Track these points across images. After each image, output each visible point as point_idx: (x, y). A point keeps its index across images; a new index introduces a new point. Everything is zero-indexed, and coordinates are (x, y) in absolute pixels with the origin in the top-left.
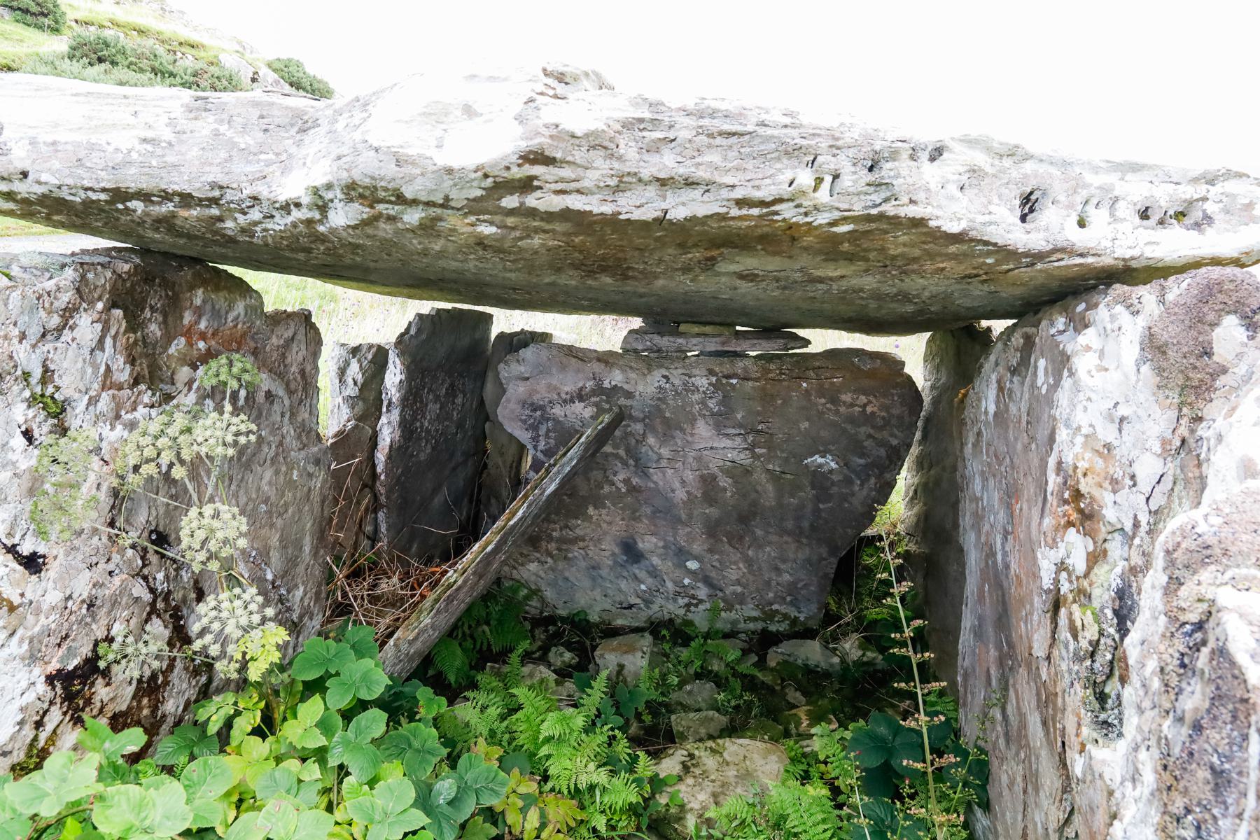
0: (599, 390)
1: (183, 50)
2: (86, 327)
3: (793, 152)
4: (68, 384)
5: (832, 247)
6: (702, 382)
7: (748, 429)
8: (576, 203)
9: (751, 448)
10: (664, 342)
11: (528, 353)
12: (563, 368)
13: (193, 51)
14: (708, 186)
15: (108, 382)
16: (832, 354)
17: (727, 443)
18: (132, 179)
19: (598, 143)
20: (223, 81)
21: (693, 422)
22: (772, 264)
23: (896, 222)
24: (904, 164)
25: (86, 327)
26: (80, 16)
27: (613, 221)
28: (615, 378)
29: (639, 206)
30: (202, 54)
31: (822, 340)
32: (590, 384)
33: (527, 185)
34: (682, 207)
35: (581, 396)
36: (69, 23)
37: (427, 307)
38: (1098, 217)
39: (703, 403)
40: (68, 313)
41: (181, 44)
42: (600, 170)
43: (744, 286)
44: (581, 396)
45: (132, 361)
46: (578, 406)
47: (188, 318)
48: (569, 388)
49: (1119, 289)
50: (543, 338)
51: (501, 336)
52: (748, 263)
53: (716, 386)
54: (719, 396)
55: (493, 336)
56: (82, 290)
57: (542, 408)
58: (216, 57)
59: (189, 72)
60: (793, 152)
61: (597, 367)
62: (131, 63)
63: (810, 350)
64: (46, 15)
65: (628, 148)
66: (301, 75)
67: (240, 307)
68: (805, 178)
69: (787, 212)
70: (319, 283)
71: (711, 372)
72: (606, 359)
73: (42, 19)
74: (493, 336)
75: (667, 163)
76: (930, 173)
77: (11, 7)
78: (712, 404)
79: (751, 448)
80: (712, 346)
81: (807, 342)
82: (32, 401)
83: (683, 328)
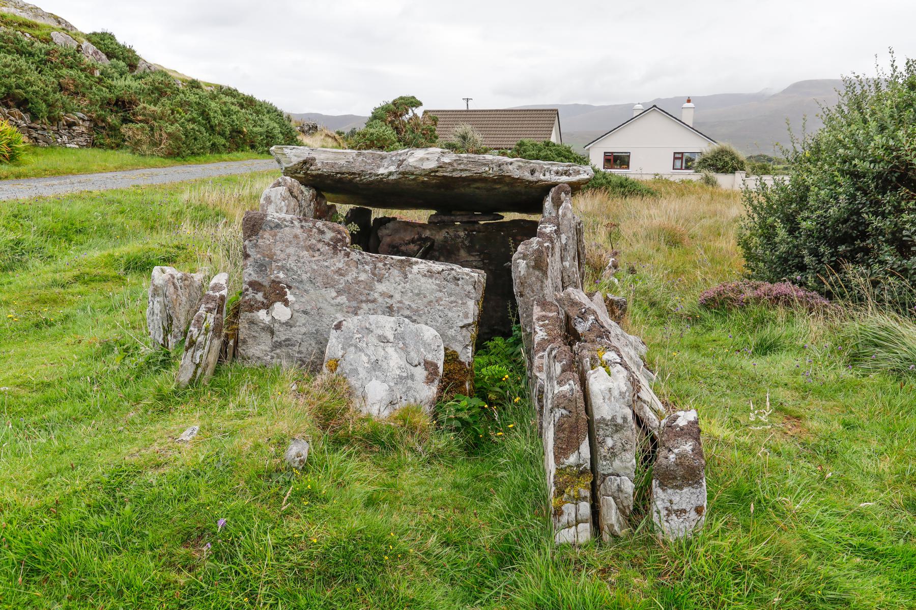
0: (420, 239)
5: (494, 181)
6: (462, 234)
7: (481, 252)
8: (445, 174)
9: (482, 260)
10: (446, 218)
11: (390, 225)
12: (405, 230)
13: (31, 31)
14: (469, 170)
16: (514, 222)
17: (472, 258)
18: (344, 170)
19: (450, 164)
21: (459, 250)
22: (483, 185)
23: (505, 176)
24: (505, 166)
27: (452, 177)
28: (427, 233)
29: (456, 174)
30: (37, 32)
31: (509, 216)
32: (416, 237)
33: (437, 171)
34: (464, 174)
35: (413, 241)
37: (352, 206)
38: (547, 174)
39: (462, 242)
41: (20, 25)
42: (450, 168)
43: (477, 191)
44: (413, 241)
46: (412, 246)
48: (408, 238)
50: (394, 219)
51: (376, 219)
52: (478, 185)
53: (468, 235)
54: (469, 239)
55: (372, 219)
57: (397, 247)
58: (49, 34)
60: (485, 165)
61: (420, 229)
63: (505, 220)
65: (455, 165)
66: (114, 46)
68: (487, 169)
69: (484, 175)
71: (465, 230)
72: (422, 226)
74: (372, 219)
75: (462, 167)
76: (510, 167)
78: (466, 242)
79: (482, 260)
80: (465, 219)
81: (502, 217)
83: (453, 212)
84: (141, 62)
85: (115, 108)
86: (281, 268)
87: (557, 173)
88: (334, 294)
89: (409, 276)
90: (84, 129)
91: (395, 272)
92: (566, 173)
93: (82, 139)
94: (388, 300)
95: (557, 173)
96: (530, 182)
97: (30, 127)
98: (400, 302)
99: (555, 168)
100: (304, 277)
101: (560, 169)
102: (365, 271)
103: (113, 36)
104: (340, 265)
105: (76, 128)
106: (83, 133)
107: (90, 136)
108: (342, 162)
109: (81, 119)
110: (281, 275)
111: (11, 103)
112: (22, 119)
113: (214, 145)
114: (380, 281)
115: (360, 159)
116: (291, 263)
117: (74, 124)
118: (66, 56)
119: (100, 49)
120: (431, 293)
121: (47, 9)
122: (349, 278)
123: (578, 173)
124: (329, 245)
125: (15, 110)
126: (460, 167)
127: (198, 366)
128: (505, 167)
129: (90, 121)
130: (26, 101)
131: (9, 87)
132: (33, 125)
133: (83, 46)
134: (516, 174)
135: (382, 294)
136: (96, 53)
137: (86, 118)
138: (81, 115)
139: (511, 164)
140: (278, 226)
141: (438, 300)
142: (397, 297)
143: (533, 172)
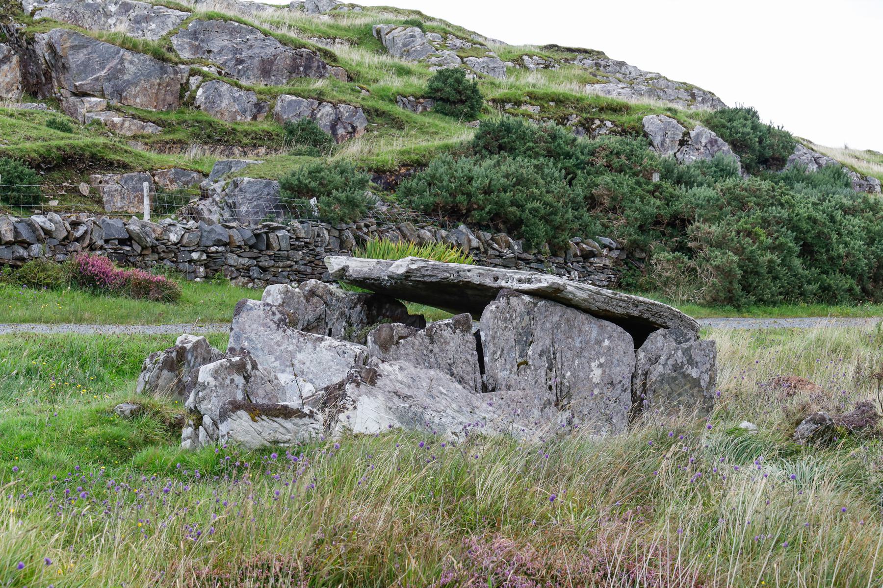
1: (603, 116)
2: (359, 307)
3: (445, 271)
4: (353, 320)
13: (614, 117)
15: (361, 322)
18: (367, 276)
20: (623, 157)
25: (359, 307)
26: (498, 93)
36: (485, 104)
40: (356, 304)
45: (367, 318)
47: (384, 311)
49: (593, 308)
56: (359, 299)
59: (586, 151)
62: (529, 149)
64: (462, 102)
67: (399, 311)
70: (434, 309)
73: (460, 107)
75: (428, 272)
77: (434, 99)
82: (346, 322)
84: (800, 151)
85: (669, 230)
86: (247, 339)
87: (520, 281)
88: (273, 360)
89: (318, 349)
90: (607, 262)
91: (310, 345)
92: (529, 281)
93: (602, 277)
94: (302, 366)
95: (520, 281)
96: (491, 288)
97: (519, 259)
98: (308, 368)
99: (517, 276)
100: (259, 346)
101: (523, 277)
102: (293, 344)
103: (755, 113)
104: (279, 338)
105: (596, 260)
106: (605, 267)
107: (616, 272)
108: (366, 269)
109: (604, 246)
110: (246, 344)
111: (501, 226)
112: (509, 246)
113: (825, 289)
114: (300, 351)
115: (378, 267)
116: (253, 336)
117: (592, 254)
118: (618, 154)
119: (722, 136)
120: (327, 362)
121: (676, 76)
122: (282, 348)
123: (540, 281)
124: (275, 323)
125: (503, 235)
126: (426, 273)
127: (146, 383)
128: (462, 273)
129: (622, 249)
130: (520, 222)
131: (500, 204)
132: (524, 256)
133: (693, 134)
134: (476, 280)
135: (300, 361)
136: (713, 142)
137: (614, 245)
138: (607, 241)
139: (469, 271)
140: (251, 309)
141: (331, 367)
142: (308, 364)
143: (496, 279)
